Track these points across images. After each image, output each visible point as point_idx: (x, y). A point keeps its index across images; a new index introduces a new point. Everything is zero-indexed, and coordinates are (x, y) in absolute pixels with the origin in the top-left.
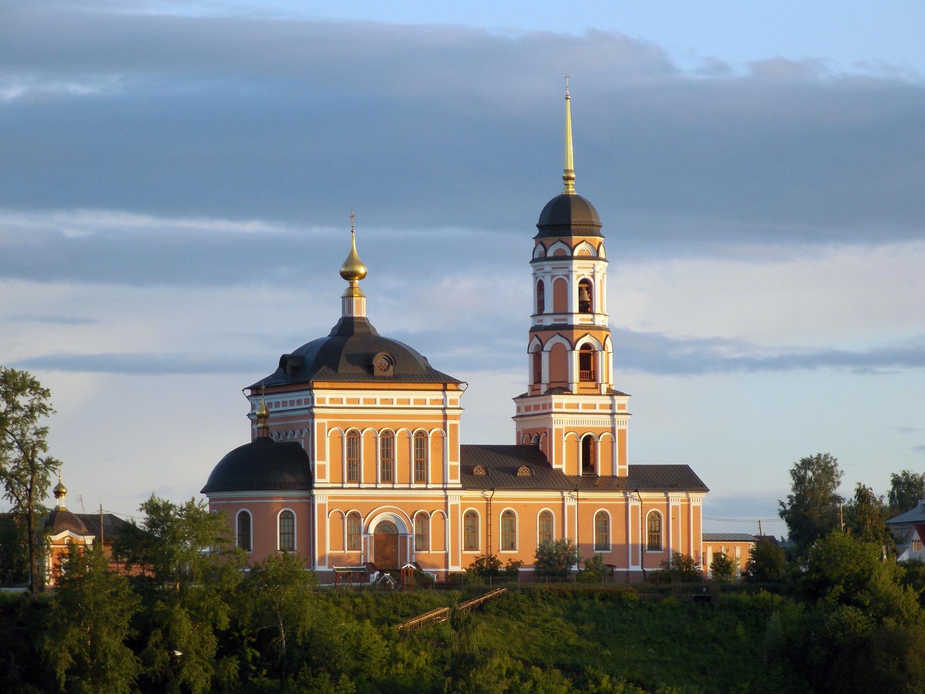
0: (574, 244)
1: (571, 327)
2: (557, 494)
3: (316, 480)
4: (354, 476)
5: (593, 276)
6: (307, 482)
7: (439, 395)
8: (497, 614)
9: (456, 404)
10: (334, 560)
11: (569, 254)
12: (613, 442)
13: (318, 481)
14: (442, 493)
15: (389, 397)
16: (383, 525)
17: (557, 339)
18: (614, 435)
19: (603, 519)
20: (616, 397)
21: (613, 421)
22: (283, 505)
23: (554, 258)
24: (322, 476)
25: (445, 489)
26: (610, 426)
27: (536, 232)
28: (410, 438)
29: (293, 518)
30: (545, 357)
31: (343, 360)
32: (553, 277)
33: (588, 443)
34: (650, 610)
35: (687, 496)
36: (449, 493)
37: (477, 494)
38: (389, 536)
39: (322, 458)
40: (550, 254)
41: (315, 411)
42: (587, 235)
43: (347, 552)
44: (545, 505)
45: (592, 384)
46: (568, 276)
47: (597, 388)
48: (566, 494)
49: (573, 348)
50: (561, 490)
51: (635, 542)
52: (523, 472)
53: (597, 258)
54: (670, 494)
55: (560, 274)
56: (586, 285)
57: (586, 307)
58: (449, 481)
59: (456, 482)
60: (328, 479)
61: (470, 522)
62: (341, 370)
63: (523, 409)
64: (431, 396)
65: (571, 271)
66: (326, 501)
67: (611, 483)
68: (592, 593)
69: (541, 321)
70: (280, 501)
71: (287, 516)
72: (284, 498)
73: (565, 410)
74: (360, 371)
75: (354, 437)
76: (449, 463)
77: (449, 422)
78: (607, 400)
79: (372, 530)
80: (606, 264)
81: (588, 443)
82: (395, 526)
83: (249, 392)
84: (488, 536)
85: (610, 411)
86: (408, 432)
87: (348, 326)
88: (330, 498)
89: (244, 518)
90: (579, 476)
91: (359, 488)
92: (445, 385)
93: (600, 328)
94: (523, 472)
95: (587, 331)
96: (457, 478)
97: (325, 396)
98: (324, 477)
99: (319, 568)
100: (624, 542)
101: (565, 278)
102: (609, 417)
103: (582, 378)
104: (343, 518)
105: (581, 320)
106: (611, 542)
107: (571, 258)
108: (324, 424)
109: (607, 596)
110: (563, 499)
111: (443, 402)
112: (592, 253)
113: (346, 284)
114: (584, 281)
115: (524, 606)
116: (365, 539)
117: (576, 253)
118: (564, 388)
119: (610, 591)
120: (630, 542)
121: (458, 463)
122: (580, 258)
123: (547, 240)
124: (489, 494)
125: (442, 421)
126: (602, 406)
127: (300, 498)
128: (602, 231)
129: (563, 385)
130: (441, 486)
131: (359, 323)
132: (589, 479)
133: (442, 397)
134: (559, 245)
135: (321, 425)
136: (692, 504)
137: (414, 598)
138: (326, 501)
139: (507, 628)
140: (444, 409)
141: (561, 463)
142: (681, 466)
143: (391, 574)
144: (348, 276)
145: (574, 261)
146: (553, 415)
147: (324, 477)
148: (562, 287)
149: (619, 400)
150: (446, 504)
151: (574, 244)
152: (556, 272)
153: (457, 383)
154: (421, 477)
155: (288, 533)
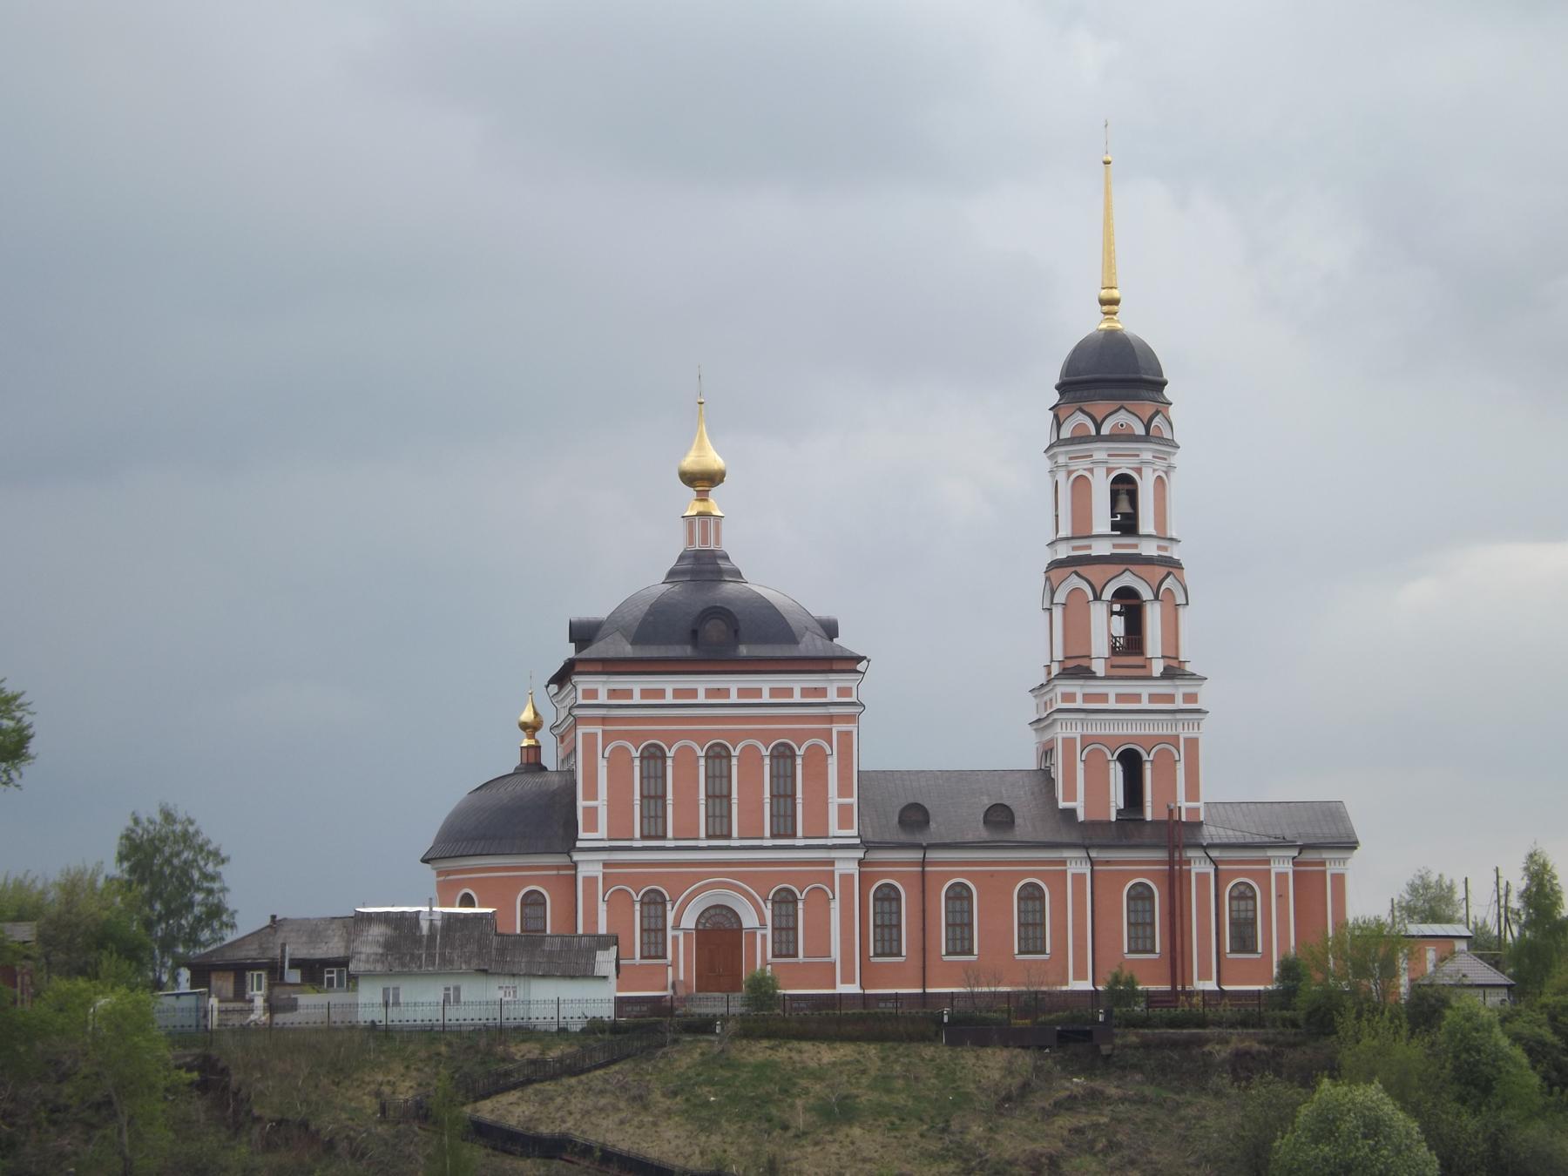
3: (581, 835)
23: (1111, 438)
24: (592, 825)
29: (899, 899)
39: (592, 793)
40: (1105, 430)
44: (962, 874)
60: (602, 831)
69: (1089, 547)
71: (1141, 896)
76: (834, 800)
79: (689, 921)
83: (554, 688)
87: (703, 567)
88: (606, 865)
93: (1149, 561)
98: (595, 829)
99: (1200, 985)
101: (1087, 474)
116: (675, 939)
127: (558, 868)
134: (1080, 418)
141: (841, 806)
147: (595, 829)
152: (1114, 462)
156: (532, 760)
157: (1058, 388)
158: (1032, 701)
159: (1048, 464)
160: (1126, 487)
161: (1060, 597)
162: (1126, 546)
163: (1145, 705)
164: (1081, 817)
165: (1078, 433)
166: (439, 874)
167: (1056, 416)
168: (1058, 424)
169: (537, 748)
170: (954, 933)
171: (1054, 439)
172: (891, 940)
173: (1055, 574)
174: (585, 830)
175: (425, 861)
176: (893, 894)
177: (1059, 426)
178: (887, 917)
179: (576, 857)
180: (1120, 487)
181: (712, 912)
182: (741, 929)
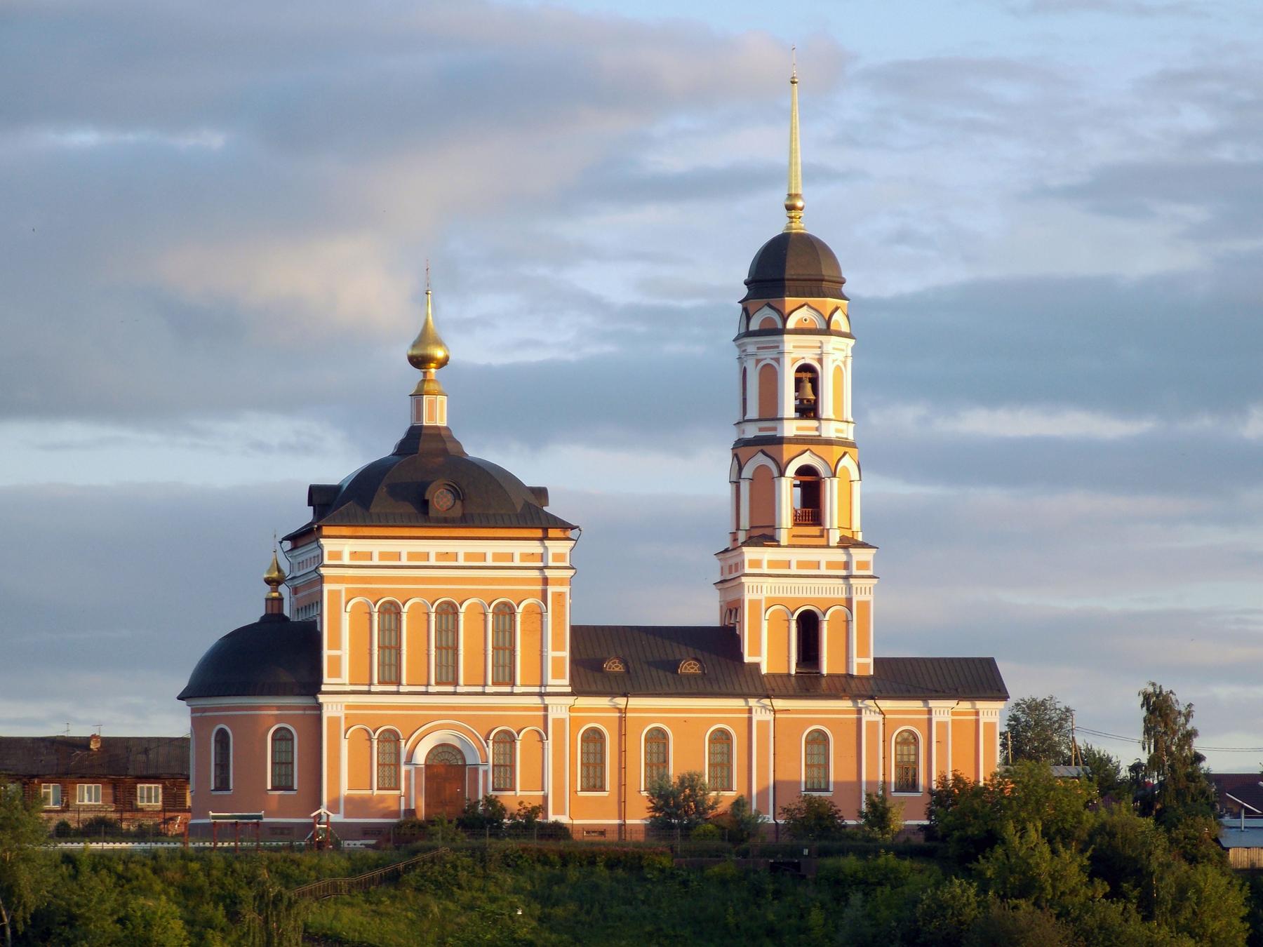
0: (787, 311)
1: (780, 441)
2: (738, 703)
3: (326, 679)
4: (391, 675)
5: (820, 361)
6: (311, 685)
7: (535, 547)
8: (418, 889)
9: (564, 561)
10: (355, 805)
11: (780, 326)
12: (848, 622)
13: (328, 682)
14: (536, 701)
15: (481, 550)
16: (442, 749)
17: (761, 459)
18: (851, 611)
19: (818, 740)
20: (852, 551)
21: (849, 588)
22: (278, 719)
24: (336, 672)
25: (541, 695)
26: (844, 596)
27: (744, 291)
28: (485, 615)
29: (292, 739)
30: (745, 487)
31: (383, 490)
32: (758, 361)
33: (809, 624)
34: (685, 883)
35: (974, 707)
36: (548, 700)
37: (603, 702)
38: (447, 769)
39: (336, 644)
41: (323, 571)
42: (812, 296)
43: (376, 792)
45: (815, 530)
46: (777, 360)
47: (822, 536)
48: (753, 702)
49: (782, 474)
50: (745, 696)
51: (873, 778)
52: (689, 667)
53: (827, 331)
54: (932, 703)
55: (767, 357)
56: (808, 375)
57: (808, 410)
58: (550, 681)
59: (564, 683)
60: (345, 677)
61: (718, 747)
62: (374, 509)
63: (726, 570)
64: (520, 548)
65: (782, 353)
66: (341, 713)
67: (845, 687)
68: (594, 856)
69: (744, 432)
70: (272, 712)
71: (282, 737)
72: (279, 708)
73: (765, 570)
74: (409, 508)
75: (392, 611)
76: (551, 654)
77: (551, 590)
78: (839, 556)
79: (421, 757)
80: (852, 342)
81: (809, 624)
82: (460, 752)
83: (288, 545)
84: (622, 768)
85: (844, 573)
86: (483, 605)
88: (348, 707)
89: (222, 738)
90: (789, 675)
91: (398, 693)
92: (545, 530)
93: (829, 442)
94: (689, 667)
95: (806, 447)
96: (563, 677)
97: (340, 548)
98: (338, 675)
100: (854, 778)
102: (841, 581)
103: (799, 520)
104: (370, 739)
105: (798, 429)
106: (832, 779)
107: (782, 331)
108: (339, 592)
109: (620, 862)
110: (750, 711)
111: (542, 557)
112: (820, 325)
113: (417, 374)
114: (805, 368)
115: (463, 875)
116: (408, 773)
117: (791, 324)
118: (764, 536)
119: (626, 853)
120: (864, 778)
121: (566, 654)
122: (797, 331)
123: (753, 304)
124: (621, 702)
125: (540, 588)
126: (830, 565)
127: (305, 708)
128: (845, 289)
129: (767, 532)
130: (537, 689)
131: (430, 435)
132: (808, 678)
133: (541, 550)
134: (767, 312)
135: (335, 594)
136: (983, 719)
137: (293, 861)
138: (341, 713)
139: (424, 911)
140: (846, 578)
142: (981, 660)
143: (459, 834)
144: (419, 362)
145: (786, 337)
146: (744, 579)
148: (770, 377)
149: (858, 555)
150: (546, 718)
151: (787, 311)
153: (566, 526)
154: (506, 675)
155: (505, 766)
156: (276, 611)
157: (746, 283)
158: (716, 563)
159: (736, 352)
160: (809, 375)
161: (748, 472)
162: (806, 427)
163: (823, 571)
164: (764, 670)
165: (767, 326)
166: (193, 711)
167: (745, 310)
168: (747, 315)
169: (280, 600)
170: (651, 771)
171: (743, 330)
172: (722, 777)
173: (743, 452)
174: (554, 677)
175: (180, 698)
176: (289, 736)
177: (748, 319)
178: (592, 757)
179: (321, 698)
180: (803, 375)
181: (440, 750)
182: (465, 765)
